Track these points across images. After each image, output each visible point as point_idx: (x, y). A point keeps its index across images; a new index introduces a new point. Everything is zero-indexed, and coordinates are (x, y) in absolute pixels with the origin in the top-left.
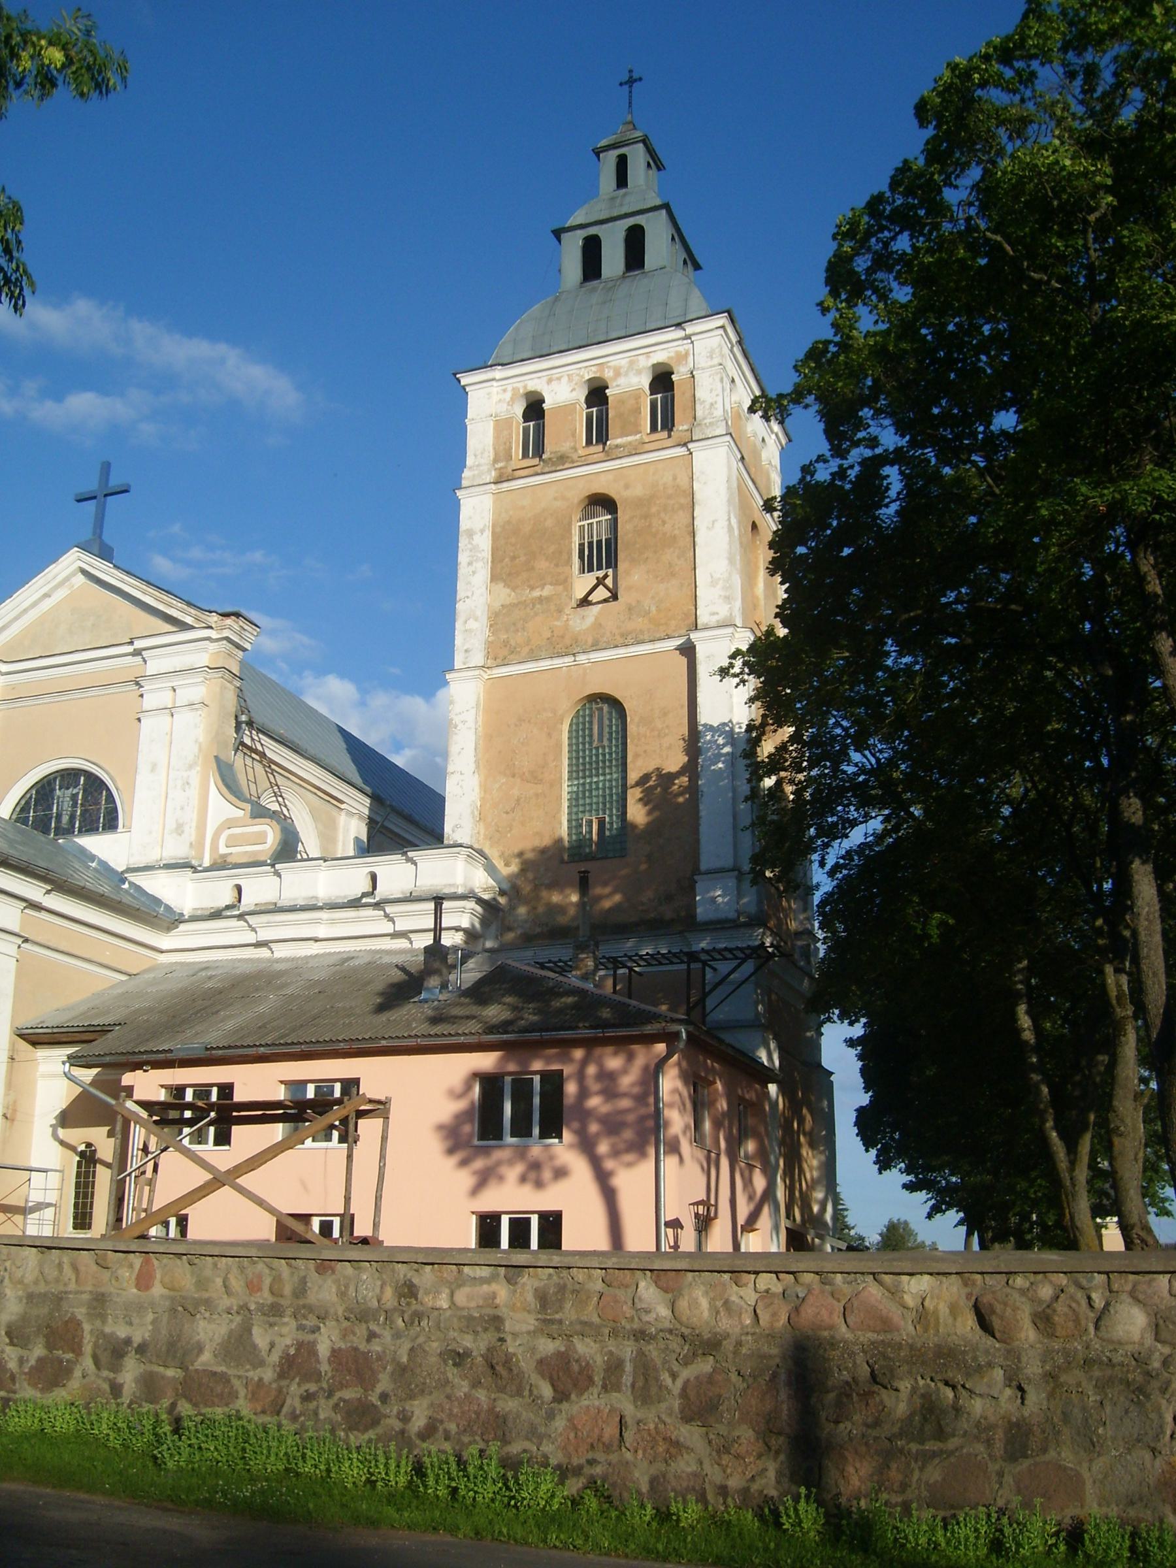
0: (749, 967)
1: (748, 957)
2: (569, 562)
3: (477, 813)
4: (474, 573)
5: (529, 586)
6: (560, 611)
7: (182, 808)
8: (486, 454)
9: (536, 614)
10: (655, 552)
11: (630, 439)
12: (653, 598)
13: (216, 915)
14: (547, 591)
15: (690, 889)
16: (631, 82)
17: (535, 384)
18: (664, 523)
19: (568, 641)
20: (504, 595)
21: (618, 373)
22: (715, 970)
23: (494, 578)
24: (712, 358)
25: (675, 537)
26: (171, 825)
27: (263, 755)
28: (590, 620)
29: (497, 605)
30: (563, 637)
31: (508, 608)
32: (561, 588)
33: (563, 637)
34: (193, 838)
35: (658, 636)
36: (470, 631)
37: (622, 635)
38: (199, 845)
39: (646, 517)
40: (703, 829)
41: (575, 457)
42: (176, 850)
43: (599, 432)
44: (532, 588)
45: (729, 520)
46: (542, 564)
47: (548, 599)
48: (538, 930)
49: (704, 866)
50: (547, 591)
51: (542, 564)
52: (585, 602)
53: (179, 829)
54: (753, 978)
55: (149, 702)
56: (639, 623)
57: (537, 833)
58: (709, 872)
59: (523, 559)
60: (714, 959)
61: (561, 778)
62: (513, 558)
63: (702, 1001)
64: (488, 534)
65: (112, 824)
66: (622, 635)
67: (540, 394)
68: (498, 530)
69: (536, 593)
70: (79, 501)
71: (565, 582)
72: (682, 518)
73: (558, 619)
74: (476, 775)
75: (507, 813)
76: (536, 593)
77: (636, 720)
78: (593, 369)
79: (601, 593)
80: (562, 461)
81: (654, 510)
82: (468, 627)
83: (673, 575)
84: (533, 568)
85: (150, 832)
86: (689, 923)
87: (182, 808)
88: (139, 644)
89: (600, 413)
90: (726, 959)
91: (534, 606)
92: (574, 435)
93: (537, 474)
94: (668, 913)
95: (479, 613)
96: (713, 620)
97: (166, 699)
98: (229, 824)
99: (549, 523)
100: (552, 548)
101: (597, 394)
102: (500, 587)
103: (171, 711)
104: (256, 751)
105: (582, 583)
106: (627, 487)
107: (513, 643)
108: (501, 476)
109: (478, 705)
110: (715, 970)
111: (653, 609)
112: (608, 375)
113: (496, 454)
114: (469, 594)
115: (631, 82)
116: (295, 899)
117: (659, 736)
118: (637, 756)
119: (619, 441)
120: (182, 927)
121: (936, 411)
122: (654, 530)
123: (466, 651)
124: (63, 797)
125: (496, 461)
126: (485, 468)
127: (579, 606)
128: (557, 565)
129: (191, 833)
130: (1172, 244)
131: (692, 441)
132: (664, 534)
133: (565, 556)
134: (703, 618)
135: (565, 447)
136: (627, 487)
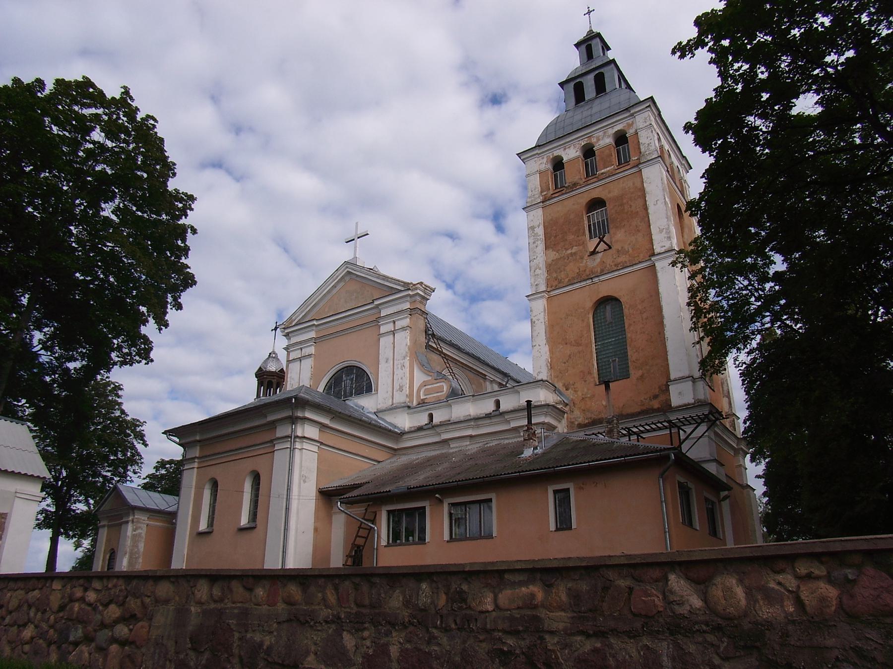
0: (703, 428)
1: (703, 421)
2: (584, 233)
3: (549, 365)
4: (536, 246)
5: (565, 249)
6: (582, 258)
7: (402, 378)
8: (537, 190)
9: (570, 262)
10: (628, 221)
11: (608, 169)
12: (629, 244)
13: (420, 429)
14: (575, 249)
15: (666, 390)
16: (589, 12)
17: (557, 153)
18: (631, 206)
19: (587, 272)
20: (553, 255)
21: (598, 140)
22: (685, 432)
23: (547, 248)
24: (646, 122)
25: (637, 212)
26: (396, 387)
27: (442, 352)
28: (598, 260)
29: (550, 261)
30: (585, 271)
31: (556, 261)
32: (581, 247)
33: (585, 271)
34: (408, 393)
35: (634, 263)
36: (538, 275)
37: (615, 265)
38: (410, 395)
39: (622, 205)
40: (669, 345)
41: (581, 182)
42: (400, 398)
43: (590, 172)
44: (567, 249)
45: (665, 199)
46: (571, 237)
47: (575, 254)
48: (587, 421)
49: (672, 377)
50: (575, 249)
51: (571, 237)
52: (594, 253)
53: (401, 389)
54: (706, 434)
55: (383, 329)
56: (623, 258)
57: (581, 371)
58: (675, 380)
59: (560, 236)
60: (684, 425)
61: (591, 341)
62: (556, 237)
63: (680, 446)
64: (542, 227)
65: (369, 389)
66: (615, 265)
67: (561, 156)
68: (546, 224)
69: (569, 252)
70: (347, 242)
71: (583, 244)
72: (640, 202)
73: (582, 263)
74: (547, 346)
75: (565, 363)
76: (569, 252)
77: (628, 307)
78: (586, 139)
79: (602, 246)
80: (575, 185)
81: (625, 201)
82: (536, 273)
83: (638, 231)
84: (566, 240)
85: (387, 392)
86: (667, 408)
87: (402, 378)
88: (376, 303)
89: (591, 161)
90: (691, 424)
91: (568, 258)
92: (580, 172)
93: (563, 194)
94: (656, 404)
95: (541, 265)
96: (663, 250)
97: (390, 327)
98: (425, 384)
99: (572, 217)
100: (575, 229)
101: (589, 152)
102: (550, 251)
103: (393, 333)
104: (437, 350)
105: (592, 244)
106: (609, 192)
107: (559, 278)
108: (545, 199)
109: (545, 310)
110: (685, 432)
111: (630, 250)
112: (594, 140)
113: (542, 189)
114: (535, 257)
115: (589, 12)
116: (459, 417)
117: (641, 313)
118: (630, 325)
119: (603, 171)
120: (405, 437)
121: (783, 302)
122: (626, 211)
123: (536, 285)
124: (346, 382)
125: (541, 192)
126: (537, 196)
127: (591, 255)
128: (578, 236)
129: (407, 390)
130: (890, 85)
131: (640, 164)
132: (632, 212)
133: (581, 231)
134: (657, 249)
135: (576, 179)
136: (609, 192)
